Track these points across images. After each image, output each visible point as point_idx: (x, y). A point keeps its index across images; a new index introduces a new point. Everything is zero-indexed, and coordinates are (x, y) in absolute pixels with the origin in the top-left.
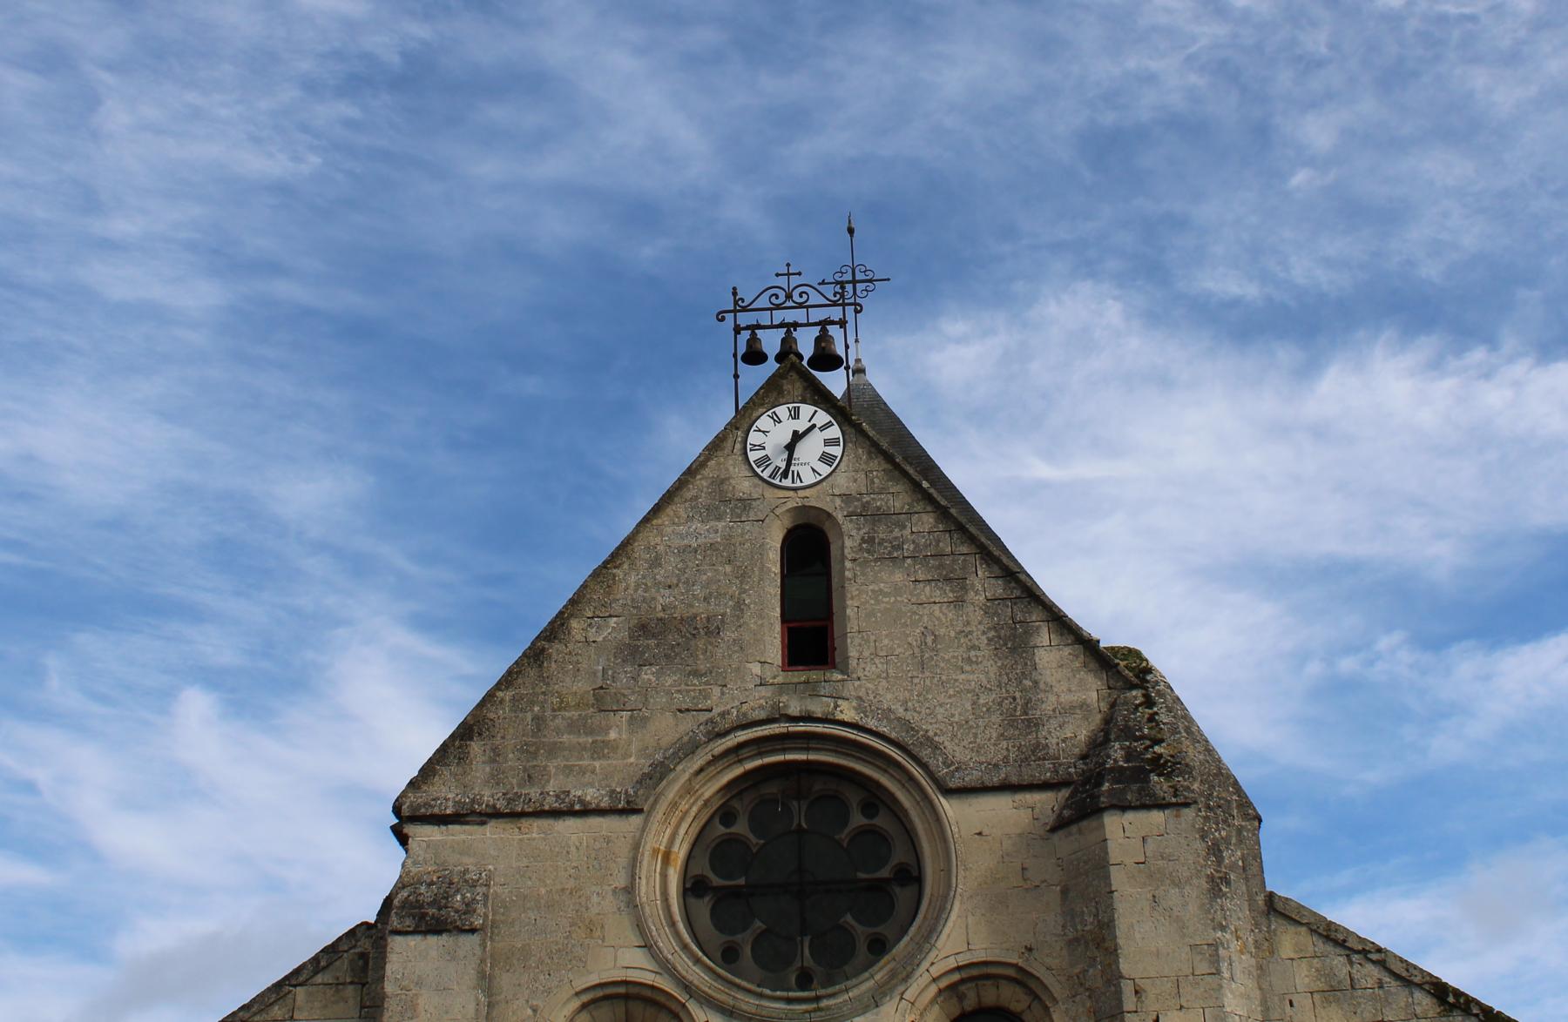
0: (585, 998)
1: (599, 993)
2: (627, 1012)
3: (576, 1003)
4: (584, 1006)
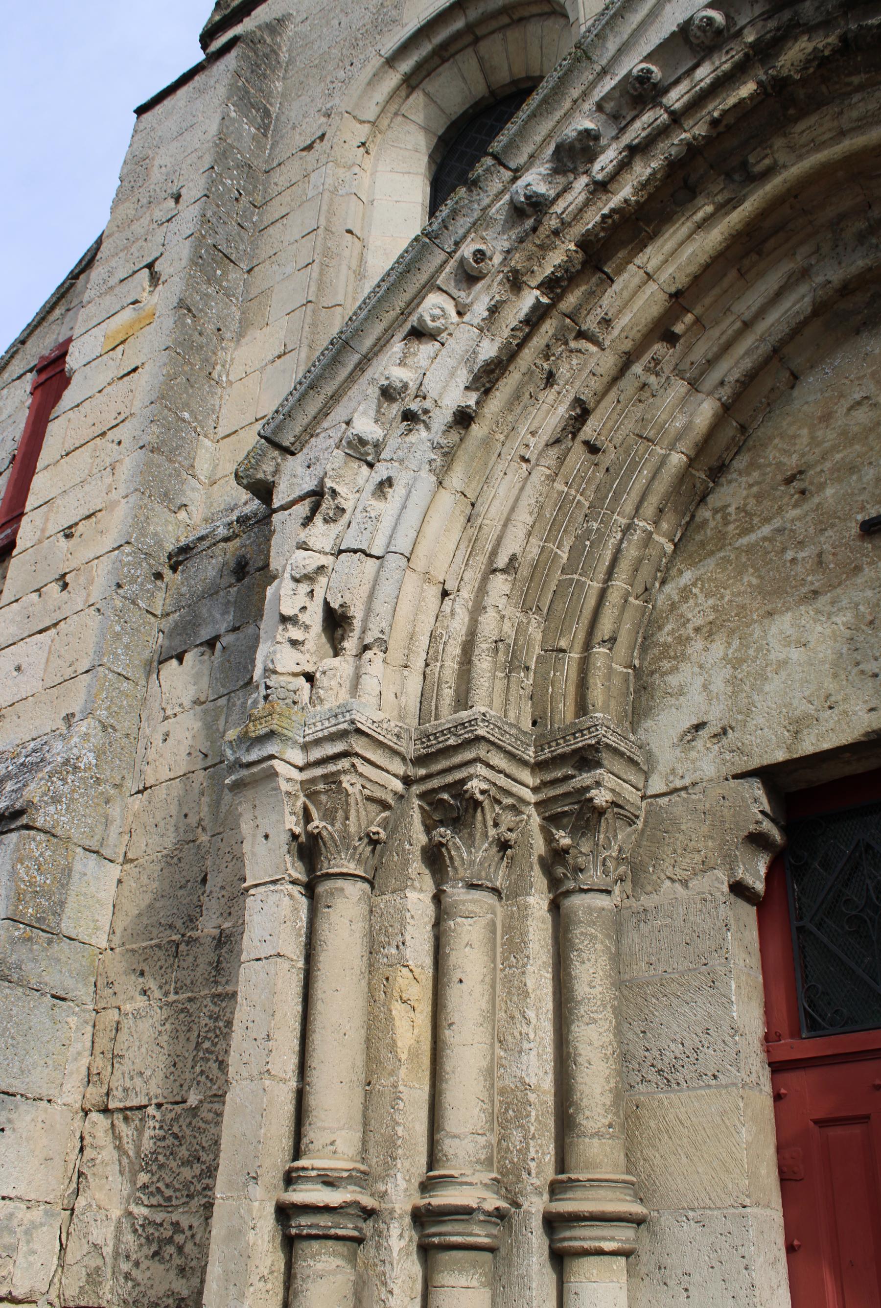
0: (406, 66)
1: (426, 49)
2: (481, 61)
3: (393, 79)
4: (411, 83)
